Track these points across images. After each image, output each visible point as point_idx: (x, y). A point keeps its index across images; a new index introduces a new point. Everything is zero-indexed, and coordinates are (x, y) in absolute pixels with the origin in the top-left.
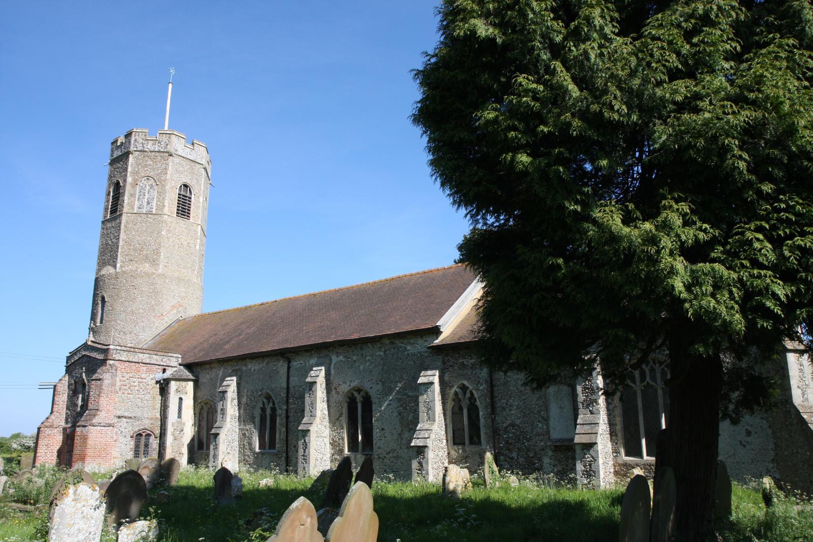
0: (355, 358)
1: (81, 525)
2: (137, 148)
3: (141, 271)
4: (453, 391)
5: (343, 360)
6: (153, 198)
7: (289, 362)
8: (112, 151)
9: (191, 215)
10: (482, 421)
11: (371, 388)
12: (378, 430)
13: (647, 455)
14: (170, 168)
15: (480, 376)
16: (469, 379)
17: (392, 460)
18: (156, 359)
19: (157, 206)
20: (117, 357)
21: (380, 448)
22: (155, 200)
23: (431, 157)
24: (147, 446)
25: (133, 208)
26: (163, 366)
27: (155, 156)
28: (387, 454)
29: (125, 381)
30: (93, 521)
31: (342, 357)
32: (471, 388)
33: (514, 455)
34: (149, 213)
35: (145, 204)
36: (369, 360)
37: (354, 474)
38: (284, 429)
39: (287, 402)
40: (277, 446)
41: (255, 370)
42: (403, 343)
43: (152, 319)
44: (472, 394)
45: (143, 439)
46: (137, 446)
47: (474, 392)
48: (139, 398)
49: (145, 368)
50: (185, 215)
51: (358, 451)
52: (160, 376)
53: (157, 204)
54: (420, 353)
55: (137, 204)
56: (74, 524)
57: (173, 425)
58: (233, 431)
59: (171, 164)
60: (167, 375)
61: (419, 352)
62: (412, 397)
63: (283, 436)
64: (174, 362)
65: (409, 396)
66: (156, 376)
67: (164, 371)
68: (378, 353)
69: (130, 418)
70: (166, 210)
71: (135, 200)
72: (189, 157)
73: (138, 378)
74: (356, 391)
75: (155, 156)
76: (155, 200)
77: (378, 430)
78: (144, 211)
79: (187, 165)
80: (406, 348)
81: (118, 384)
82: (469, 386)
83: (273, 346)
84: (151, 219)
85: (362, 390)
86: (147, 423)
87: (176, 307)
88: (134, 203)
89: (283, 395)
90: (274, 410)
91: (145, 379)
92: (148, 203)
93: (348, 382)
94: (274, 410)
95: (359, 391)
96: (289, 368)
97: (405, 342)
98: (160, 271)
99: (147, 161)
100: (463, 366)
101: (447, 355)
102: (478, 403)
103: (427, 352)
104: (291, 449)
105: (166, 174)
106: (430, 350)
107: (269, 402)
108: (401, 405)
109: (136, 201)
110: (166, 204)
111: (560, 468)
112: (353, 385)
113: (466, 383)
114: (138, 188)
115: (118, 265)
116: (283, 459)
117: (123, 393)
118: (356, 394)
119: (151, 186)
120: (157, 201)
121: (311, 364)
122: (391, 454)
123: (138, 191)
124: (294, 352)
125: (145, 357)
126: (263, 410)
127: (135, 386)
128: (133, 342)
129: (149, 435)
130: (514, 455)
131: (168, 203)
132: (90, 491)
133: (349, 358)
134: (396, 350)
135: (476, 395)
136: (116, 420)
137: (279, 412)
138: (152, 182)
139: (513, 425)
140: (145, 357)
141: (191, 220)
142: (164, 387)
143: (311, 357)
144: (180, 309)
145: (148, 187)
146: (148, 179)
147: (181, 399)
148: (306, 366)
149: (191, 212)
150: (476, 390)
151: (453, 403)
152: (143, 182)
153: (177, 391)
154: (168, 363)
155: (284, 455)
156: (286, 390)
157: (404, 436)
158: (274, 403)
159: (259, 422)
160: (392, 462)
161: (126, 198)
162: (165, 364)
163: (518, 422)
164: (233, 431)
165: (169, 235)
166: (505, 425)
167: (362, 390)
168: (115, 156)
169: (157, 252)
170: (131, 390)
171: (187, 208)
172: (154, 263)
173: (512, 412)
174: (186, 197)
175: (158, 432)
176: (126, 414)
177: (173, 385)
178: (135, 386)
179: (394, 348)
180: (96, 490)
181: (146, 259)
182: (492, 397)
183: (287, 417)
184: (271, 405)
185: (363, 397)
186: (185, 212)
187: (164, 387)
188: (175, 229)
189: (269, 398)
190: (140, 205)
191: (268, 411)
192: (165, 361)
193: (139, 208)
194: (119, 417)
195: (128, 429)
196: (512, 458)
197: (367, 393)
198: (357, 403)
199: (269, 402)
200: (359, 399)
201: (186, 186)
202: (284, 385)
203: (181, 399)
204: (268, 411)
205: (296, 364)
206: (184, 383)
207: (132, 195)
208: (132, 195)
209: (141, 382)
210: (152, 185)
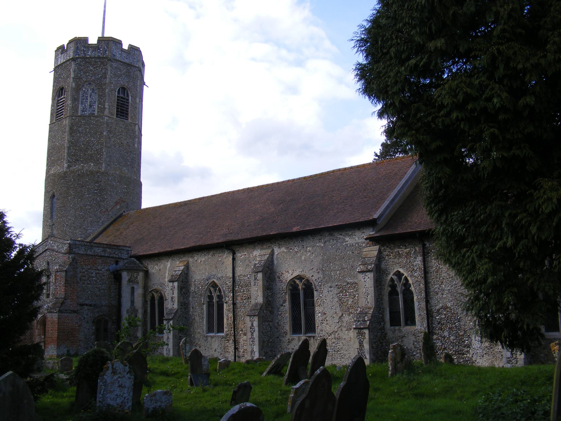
0: (296, 250)
1: (118, 391)
2: (79, 55)
3: (86, 170)
5: (285, 250)
6: (95, 102)
7: (234, 254)
10: (416, 304)
11: (312, 276)
12: (320, 314)
14: (109, 72)
15: (414, 264)
16: (403, 267)
17: (333, 340)
19: (98, 109)
21: (322, 330)
22: (97, 103)
23: (361, 58)
25: (77, 112)
26: (116, 258)
27: (95, 62)
28: (329, 336)
29: (84, 272)
30: (126, 389)
31: (283, 248)
32: (405, 274)
33: (446, 334)
34: (92, 115)
35: (88, 107)
36: (310, 251)
37: (312, 354)
38: (231, 315)
39: (233, 291)
40: (225, 330)
41: (201, 261)
42: (341, 235)
44: (406, 279)
47: (409, 278)
48: (97, 288)
49: (100, 261)
50: (123, 116)
51: (301, 333)
52: (113, 267)
53: (98, 106)
54: (358, 243)
55: (80, 107)
56: (114, 391)
58: (183, 316)
59: (109, 69)
61: (357, 243)
62: (352, 284)
63: (231, 321)
65: (348, 283)
66: (110, 268)
67: (117, 263)
68: (318, 244)
69: (91, 305)
70: (107, 112)
71: (78, 103)
73: (95, 270)
74: (298, 279)
75: (95, 62)
76: (97, 103)
77: (320, 314)
78: (87, 113)
80: (344, 239)
81: (79, 275)
82: (404, 273)
85: (304, 279)
87: (118, 203)
88: (78, 107)
91: (101, 270)
92: (91, 106)
93: (290, 271)
94: (220, 297)
95: (300, 278)
96: (234, 259)
97: (343, 234)
99: (88, 67)
100: (400, 256)
101: (383, 246)
102: (412, 288)
103: (364, 242)
104: (238, 333)
105: (106, 78)
106: (368, 241)
107: (215, 291)
108: (341, 292)
109: (80, 105)
110: (106, 106)
112: (296, 274)
113: (401, 270)
116: (231, 341)
117: (84, 284)
118: (297, 282)
119: (93, 90)
120: (99, 104)
121: (254, 255)
122: (333, 336)
123: (81, 95)
124: (238, 245)
126: (211, 297)
127: (93, 277)
128: (83, 236)
130: (446, 334)
131: (109, 105)
132: (122, 366)
133: (291, 249)
134: (335, 241)
135: (410, 282)
136: (79, 308)
139: (445, 308)
141: (129, 120)
143: (254, 249)
145: (90, 91)
146: (90, 84)
148: (249, 257)
150: (411, 276)
151: (390, 289)
153: (130, 281)
155: (233, 338)
156: (231, 279)
157: (344, 320)
160: (334, 342)
162: (117, 256)
163: (449, 305)
164: (183, 316)
165: (111, 136)
166: (437, 307)
167: (304, 279)
170: (90, 281)
171: (125, 109)
173: (444, 296)
174: (124, 99)
176: (87, 302)
177: (125, 276)
178: (93, 277)
179: (333, 240)
180: (127, 366)
182: (427, 284)
183: (234, 304)
185: (304, 284)
186: (124, 113)
188: (116, 129)
189: (214, 285)
190: (84, 108)
191: (215, 300)
193: (83, 111)
194: (82, 305)
196: (444, 337)
197: (308, 280)
199: (215, 291)
202: (231, 275)
205: (240, 255)
209: (98, 273)
210: (93, 89)
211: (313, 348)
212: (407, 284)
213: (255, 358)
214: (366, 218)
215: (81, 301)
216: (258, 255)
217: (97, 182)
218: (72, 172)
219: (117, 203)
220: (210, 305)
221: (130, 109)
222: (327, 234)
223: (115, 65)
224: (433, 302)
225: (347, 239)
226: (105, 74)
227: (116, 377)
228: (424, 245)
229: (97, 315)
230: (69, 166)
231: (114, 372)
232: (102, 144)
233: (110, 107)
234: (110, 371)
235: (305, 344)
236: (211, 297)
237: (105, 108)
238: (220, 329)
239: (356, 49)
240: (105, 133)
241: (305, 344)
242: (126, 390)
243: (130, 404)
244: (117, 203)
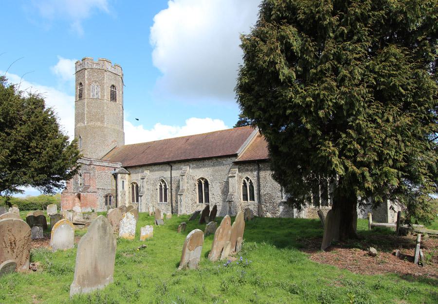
1: (129, 226)
4: (243, 180)
7: (171, 167)
8: (76, 67)
9: (117, 100)
13: (250, 200)
18: (111, 165)
20: (95, 164)
24: (110, 200)
25: (90, 96)
33: (268, 205)
38: (170, 194)
43: (104, 147)
45: (108, 197)
46: (106, 200)
52: (113, 172)
57: (121, 192)
59: (106, 75)
60: (117, 171)
64: (119, 165)
70: (105, 97)
72: (114, 72)
79: (113, 76)
83: (239, 188)
84: (99, 101)
86: (110, 192)
89: (169, 180)
90: (165, 186)
92: (97, 94)
94: (165, 186)
98: (105, 126)
101: (240, 165)
111: (286, 210)
114: (91, 86)
115: (86, 122)
119: (97, 86)
125: (106, 164)
126: (161, 186)
129: (110, 196)
130: (268, 205)
136: (97, 190)
137: (168, 187)
138: (98, 84)
140: (106, 164)
142: (115, 176)
144: (116, 143)
147: (123, 181)
149: (117, 98)
152: (93, 84)
154: (116, 166)
158: (165, 183)
159: (199, 191)
161: (86, 91)
168: (78, 70)
169: (103, 117)
172: (102, 122)
175: (115, 195)
177: (119, 176)
181: (98, 120)
184: (164, 184)
187: (115, 176)
189: (163, 181)
191: (163, 187)
192: (115, 166)
194: (98, 189)
195: (102, 194)
198: (202, 184)
200: (203, 182)
201: (113, 86)
203: (123, 181)
204: (163, 187)
206: (124, 175)
207: (89, 90)
208: (89, 90)
211: (211, 209)
212: (251, 183)
213: (370, 197)
214: (233, 153)
215: (98, 187)
216: (194, 173)
217: (102, 131)
218: (89, 126)
219: (113, 142)
220: (161, 189)
221: (117, 97)
222: (215, 159)
223: (108, 73)
224: (262, 191)
225: (224, 162)
226: (104, 78)
227: (128, 220)
228: (259, 166)
229: (106, 194)
230: (87, 123)
231: (127, 218)
232: (104, 113)
233: (107, 95)
234: (126, 217)
235: (208, 207)
236: (161, 186)
237: (104, 95)
238: (166, 200)
239: (236, 91)
240: (105, 108)
241: (208, 207)
242: (132, 226)
243: (134, 232)
244: (113, 142)
